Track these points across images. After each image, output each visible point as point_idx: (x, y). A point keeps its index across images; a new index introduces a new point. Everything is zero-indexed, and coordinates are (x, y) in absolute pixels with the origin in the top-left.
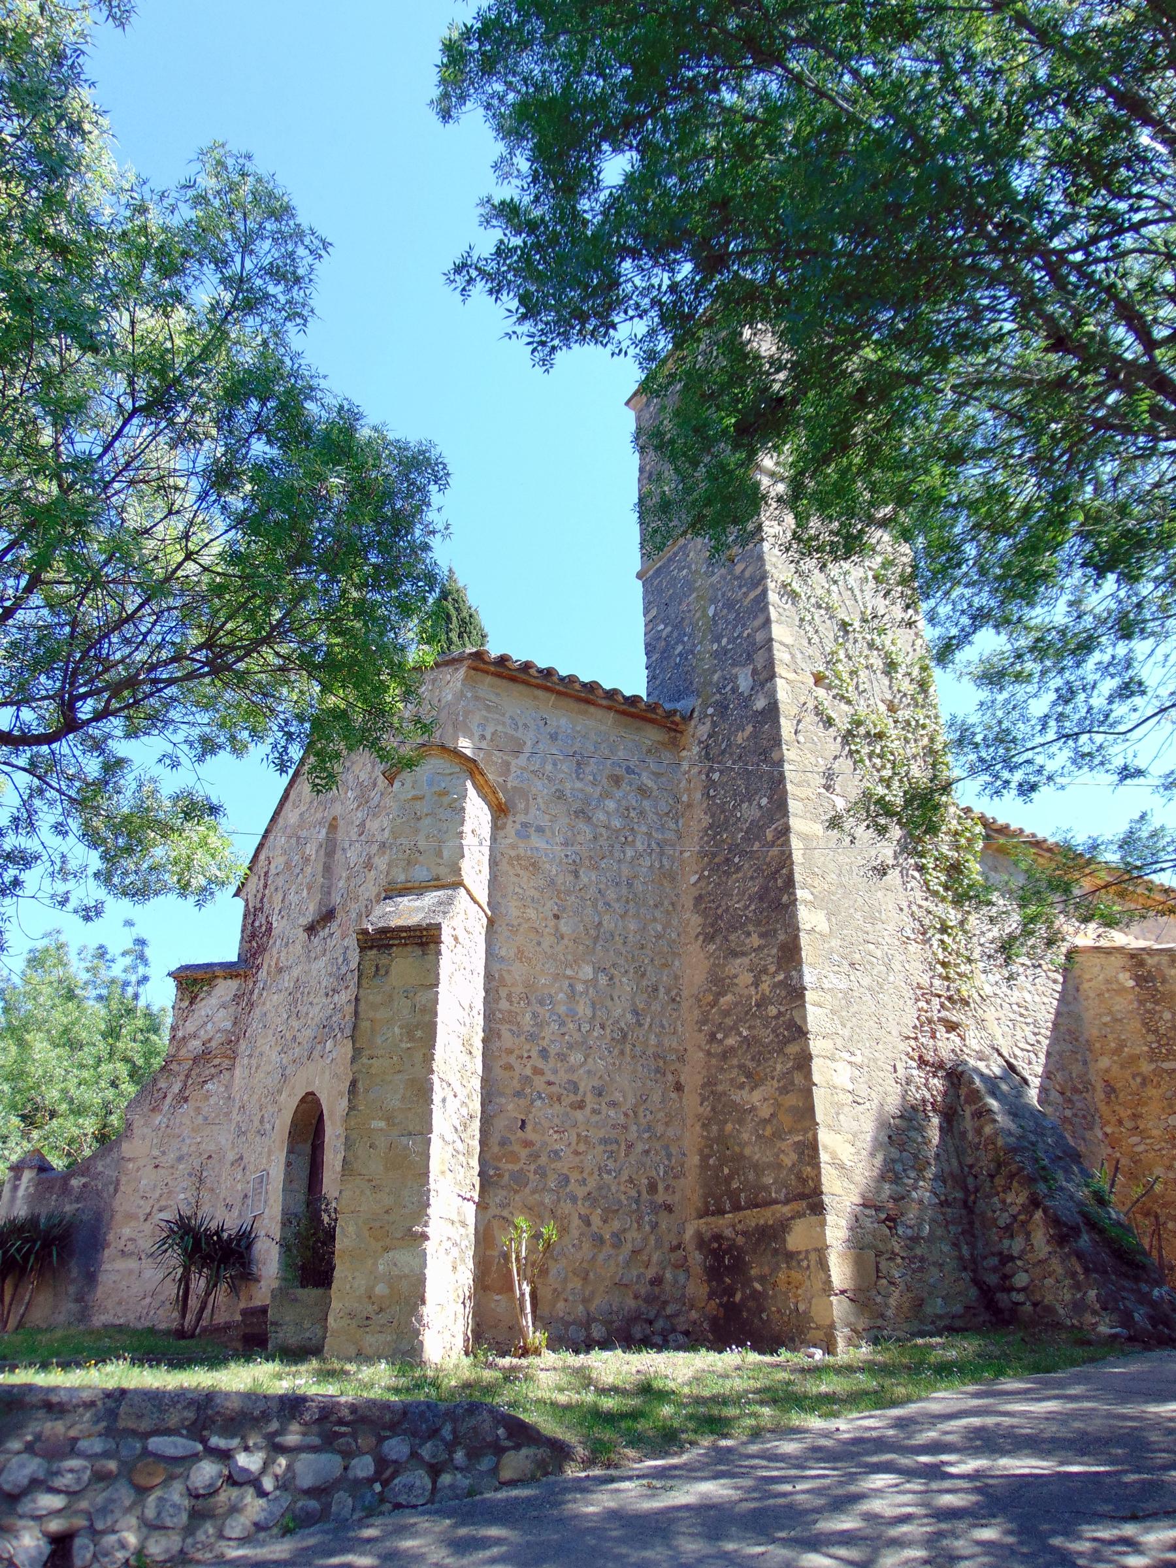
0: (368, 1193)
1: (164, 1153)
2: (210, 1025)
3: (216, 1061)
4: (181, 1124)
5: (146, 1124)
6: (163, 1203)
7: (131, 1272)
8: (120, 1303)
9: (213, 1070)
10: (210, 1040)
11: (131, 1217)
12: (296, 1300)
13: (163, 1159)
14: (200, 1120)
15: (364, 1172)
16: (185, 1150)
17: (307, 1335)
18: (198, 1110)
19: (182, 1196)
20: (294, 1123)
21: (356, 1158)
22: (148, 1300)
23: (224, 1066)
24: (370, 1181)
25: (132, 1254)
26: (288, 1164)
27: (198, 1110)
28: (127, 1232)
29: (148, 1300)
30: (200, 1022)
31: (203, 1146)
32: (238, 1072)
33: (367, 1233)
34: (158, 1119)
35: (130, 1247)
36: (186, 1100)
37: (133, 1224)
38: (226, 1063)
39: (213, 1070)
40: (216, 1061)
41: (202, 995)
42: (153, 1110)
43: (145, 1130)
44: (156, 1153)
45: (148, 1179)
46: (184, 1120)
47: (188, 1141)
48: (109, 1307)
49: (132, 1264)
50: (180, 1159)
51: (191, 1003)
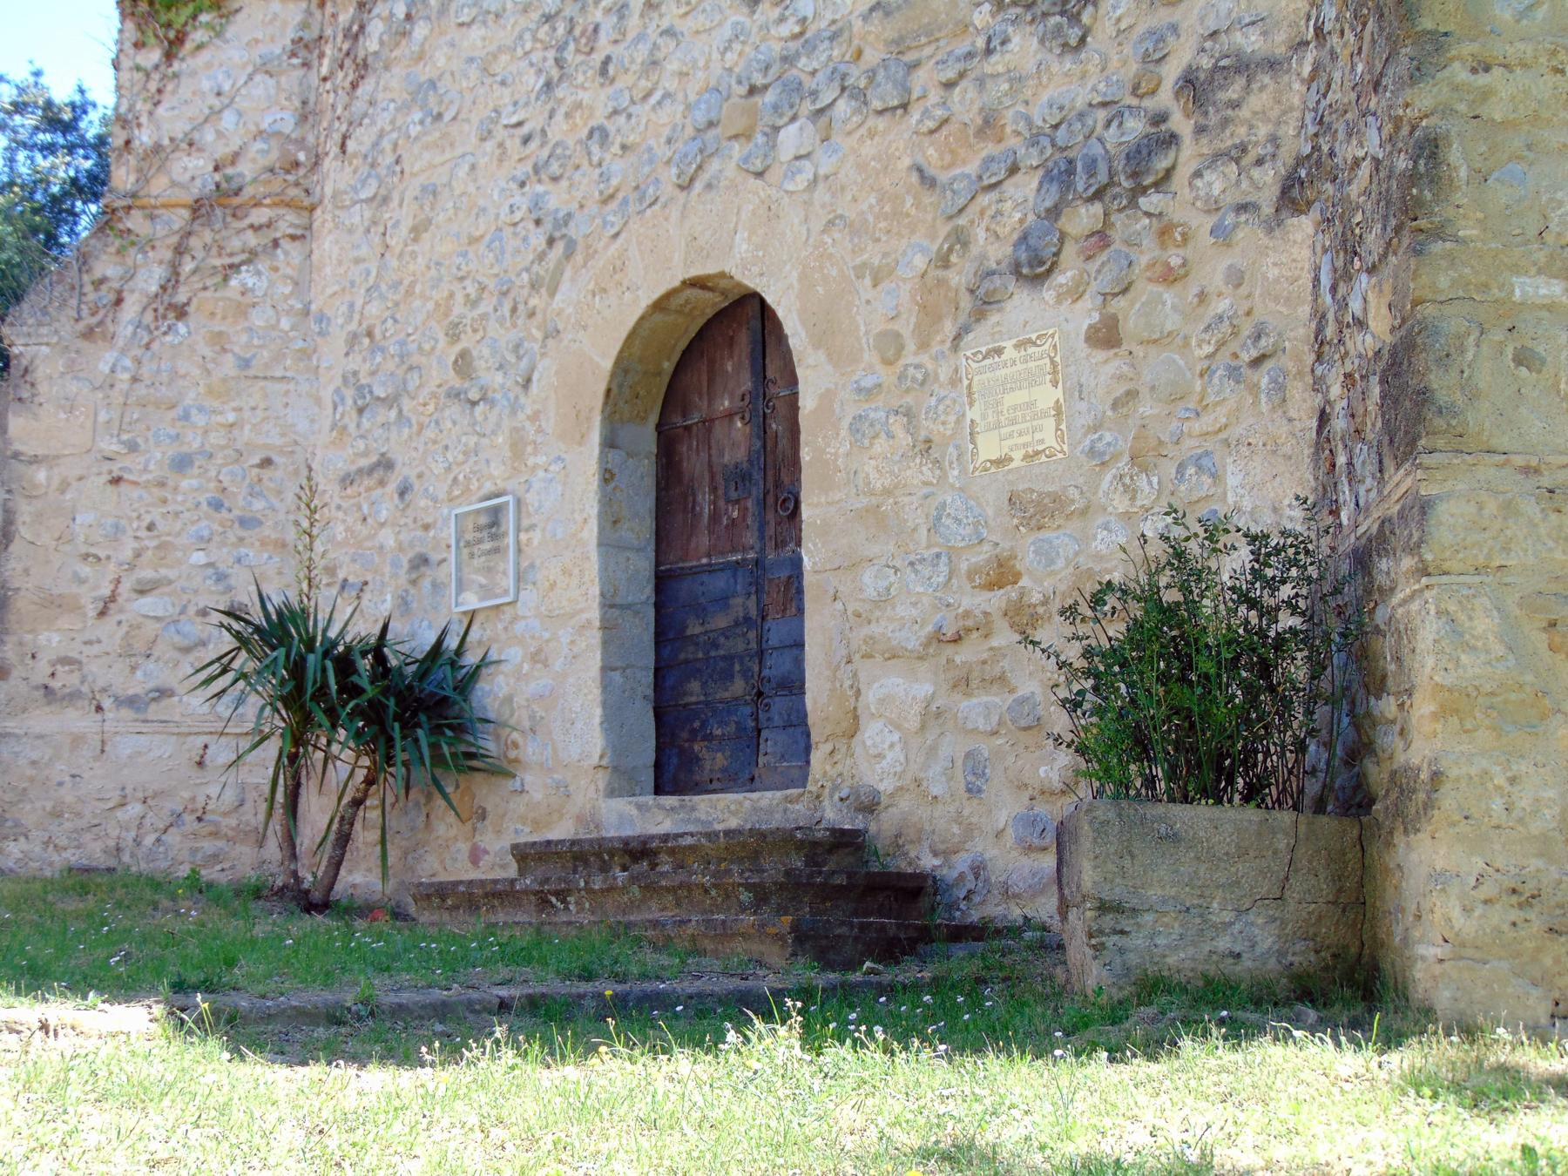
0: (1531, 508)
1: (133, 447)
2: (228, 120)
3: (259, 216)
4: (174, 375)
5: (71, 369)
6: (147, 574)
7: (77, 740)
8: (57, 814)
9: (252, 240)
10: (235, 158)
11: (56, 604)
12: (1174, 838)
13: (133, 463)
14: (229, 366)
15: (1503, 442)
16: (193, 442)
17: (1224, 943)
18: (220, 341)
19: (199, 558)
20: (622, 366)
21: (1473, 397)
22: (135, 809)
23: (283, 228)
24: (1527, 470)
25: (73, 696)
26: (607, 476)
27: (220, 341)
28: (51, 641)
29: (135, 809)
30: (199, 109)
31: (247, 433)
32: (327, 245)
33: (1540, 640)
34: (104, 360)
35: (66, 680)
36: (181, 312)
37: (65, 622)
38: (288, 221)
39: (252, 240)
40: (259, 216)
41: (198, 36)
42: (88, 335)
43: (73, 387)
44: (110, 446)
45: (93, 508)
46: (183, 366)
47: (199, 420)
48: (29, 820)
49: (78, 720)
50: (182, 463)
51: (169, 56)
